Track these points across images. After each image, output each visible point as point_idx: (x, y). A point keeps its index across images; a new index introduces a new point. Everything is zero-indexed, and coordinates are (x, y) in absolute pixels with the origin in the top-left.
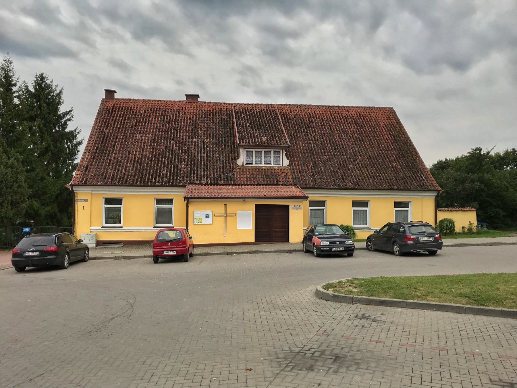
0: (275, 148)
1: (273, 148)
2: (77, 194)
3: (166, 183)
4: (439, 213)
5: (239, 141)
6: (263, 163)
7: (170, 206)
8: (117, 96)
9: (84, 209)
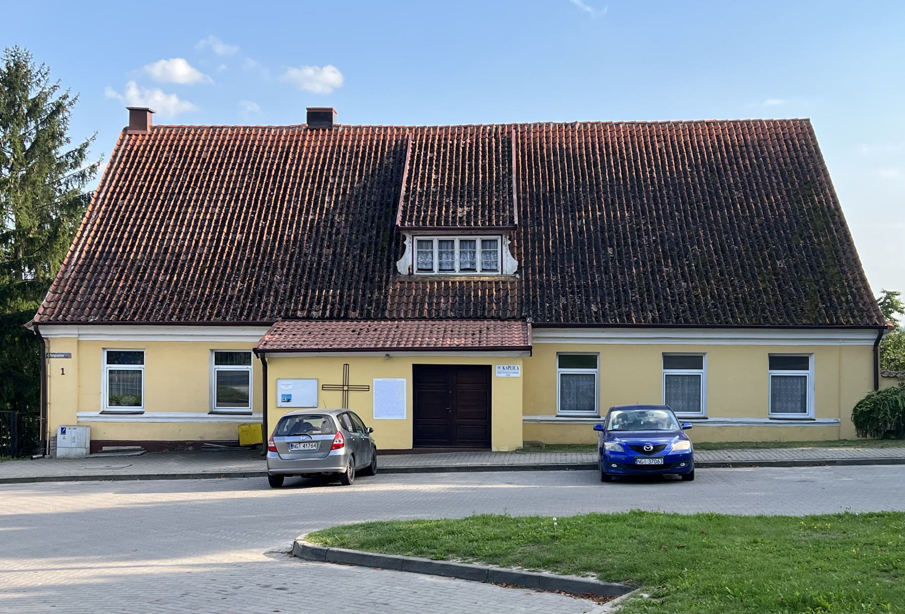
1: (480, 232)
2: (49, 342)
3: (234, 315)
5: (404, 218)
7: (246, 367)
8: (153, 121)
9: (63, 374)
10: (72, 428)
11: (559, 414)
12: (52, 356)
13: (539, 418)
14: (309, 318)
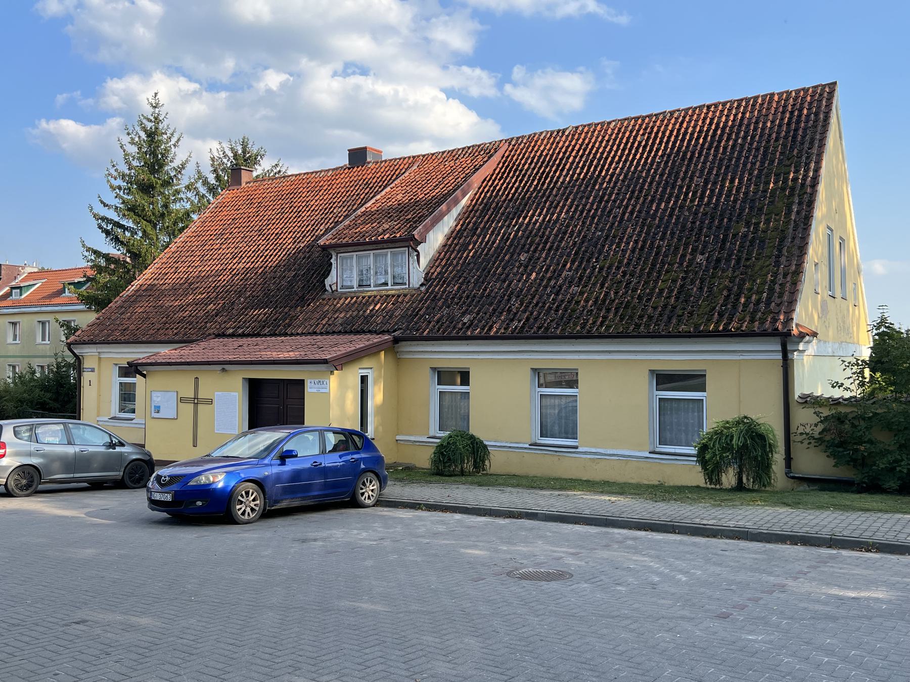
0: (393, 245)
12: (85, 370)
13: (412, 438)
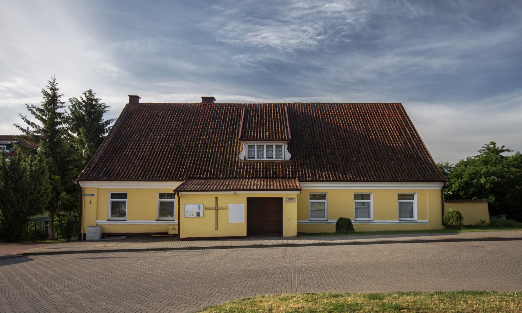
1: (275, 142)
4: (446, 204)
6: (265, 156)
8: (141, 101)
9: (90, 203)
10: (93, 227)
11: (310, 220)
14: (200, 178)
